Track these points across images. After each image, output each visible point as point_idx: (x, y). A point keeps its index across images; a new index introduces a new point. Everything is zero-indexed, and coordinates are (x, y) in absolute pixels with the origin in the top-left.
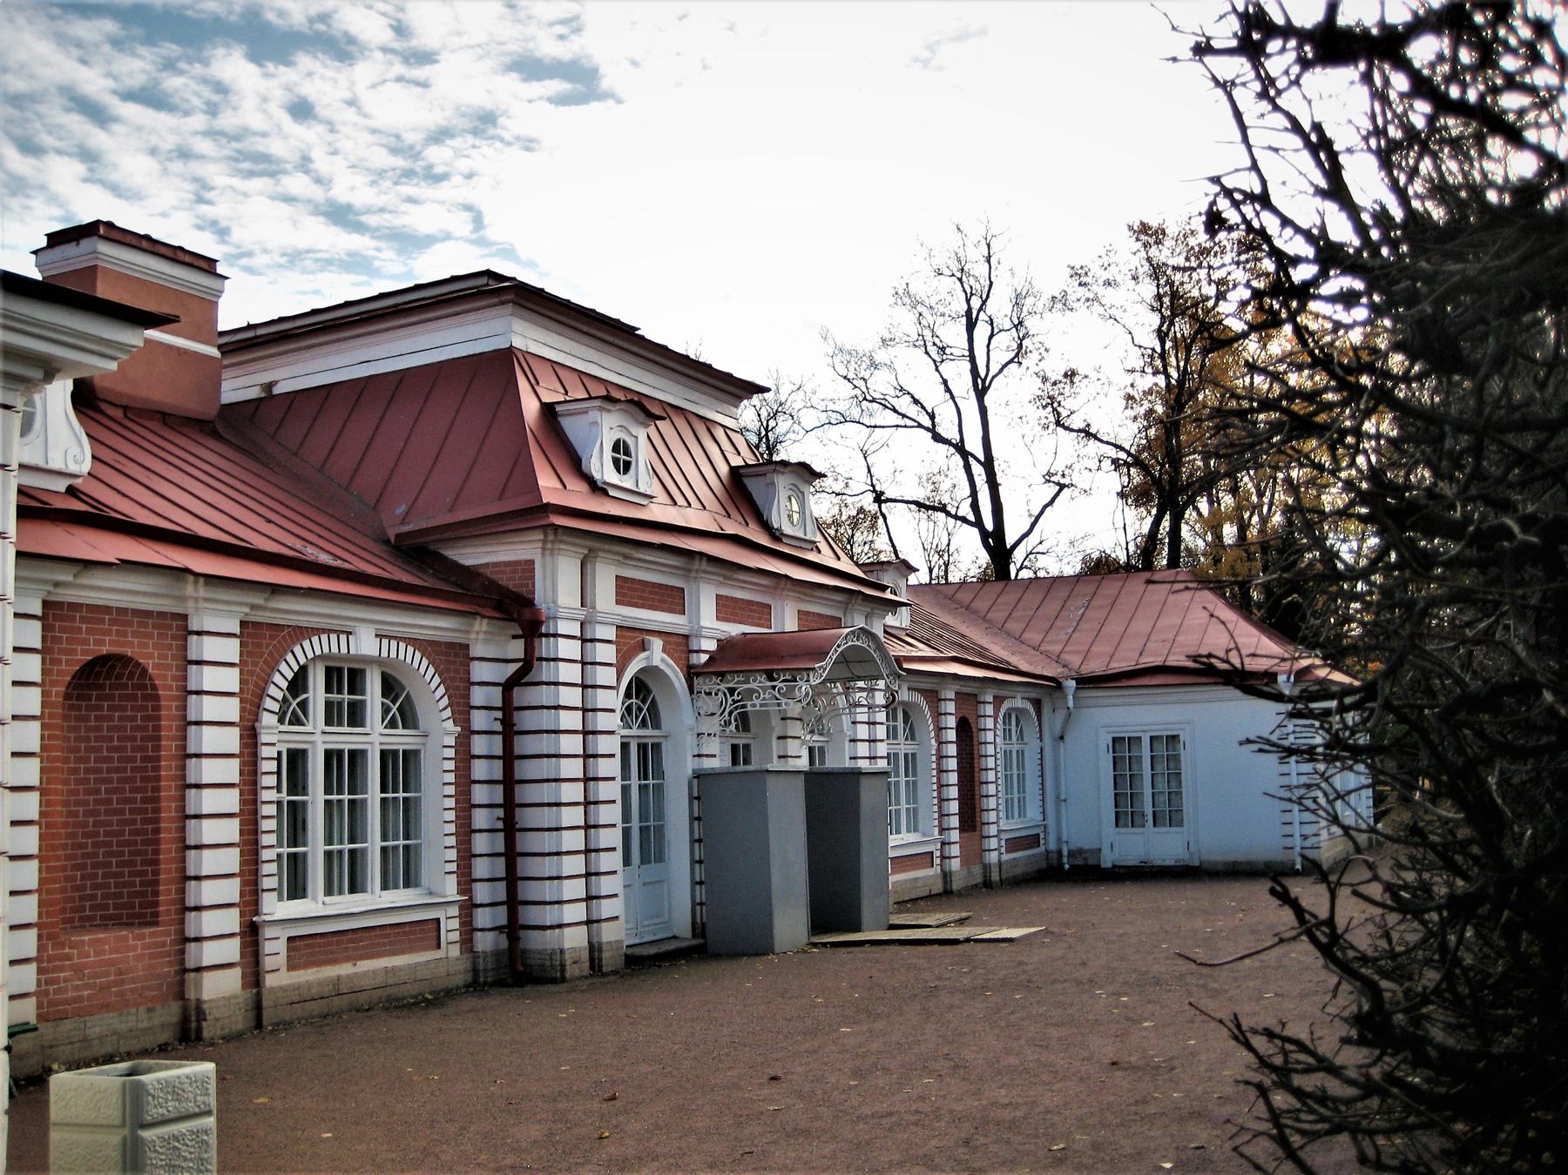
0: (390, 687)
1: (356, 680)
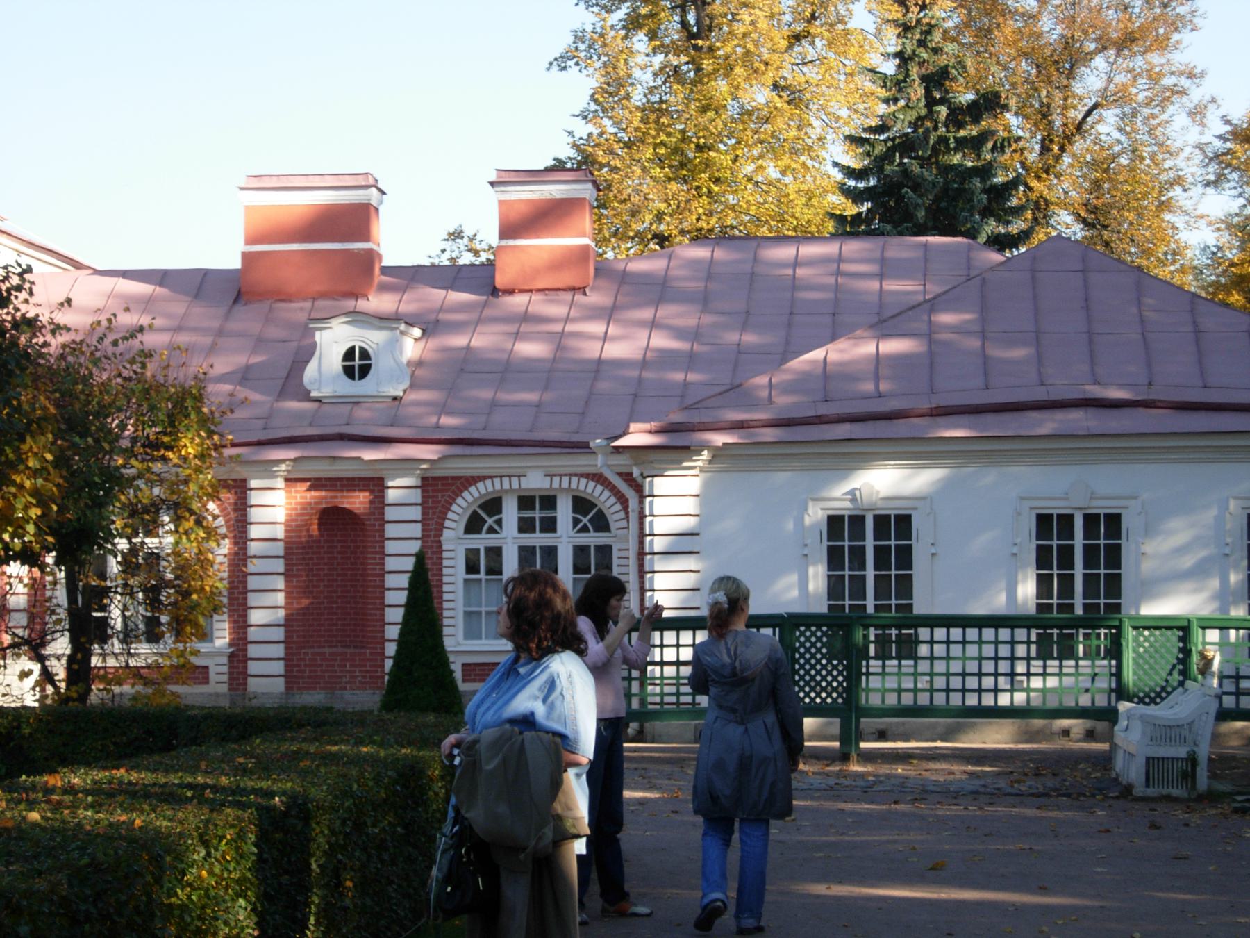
0: (581, 505)
1: (549, 502)
